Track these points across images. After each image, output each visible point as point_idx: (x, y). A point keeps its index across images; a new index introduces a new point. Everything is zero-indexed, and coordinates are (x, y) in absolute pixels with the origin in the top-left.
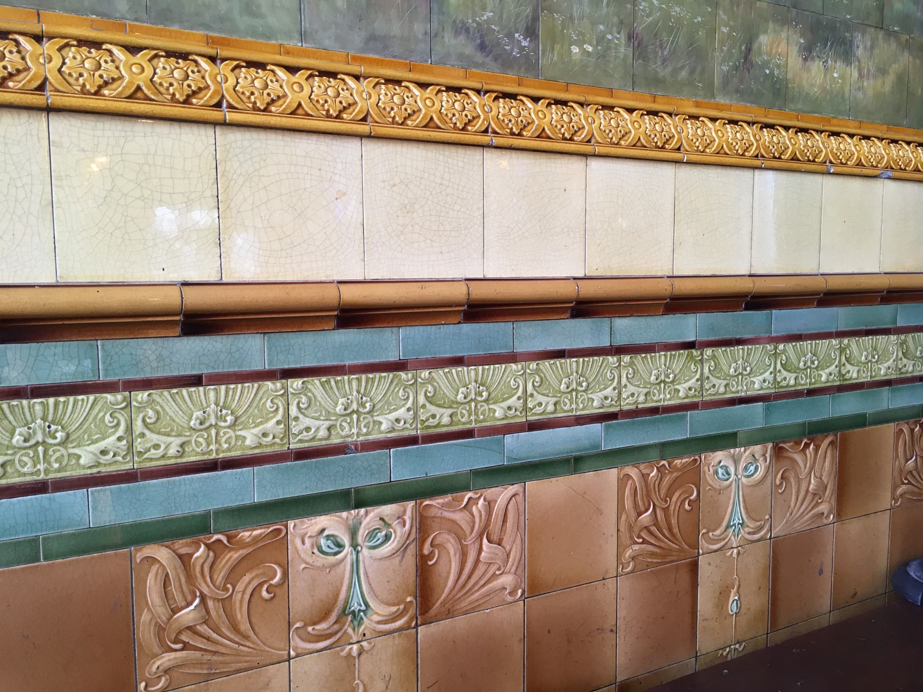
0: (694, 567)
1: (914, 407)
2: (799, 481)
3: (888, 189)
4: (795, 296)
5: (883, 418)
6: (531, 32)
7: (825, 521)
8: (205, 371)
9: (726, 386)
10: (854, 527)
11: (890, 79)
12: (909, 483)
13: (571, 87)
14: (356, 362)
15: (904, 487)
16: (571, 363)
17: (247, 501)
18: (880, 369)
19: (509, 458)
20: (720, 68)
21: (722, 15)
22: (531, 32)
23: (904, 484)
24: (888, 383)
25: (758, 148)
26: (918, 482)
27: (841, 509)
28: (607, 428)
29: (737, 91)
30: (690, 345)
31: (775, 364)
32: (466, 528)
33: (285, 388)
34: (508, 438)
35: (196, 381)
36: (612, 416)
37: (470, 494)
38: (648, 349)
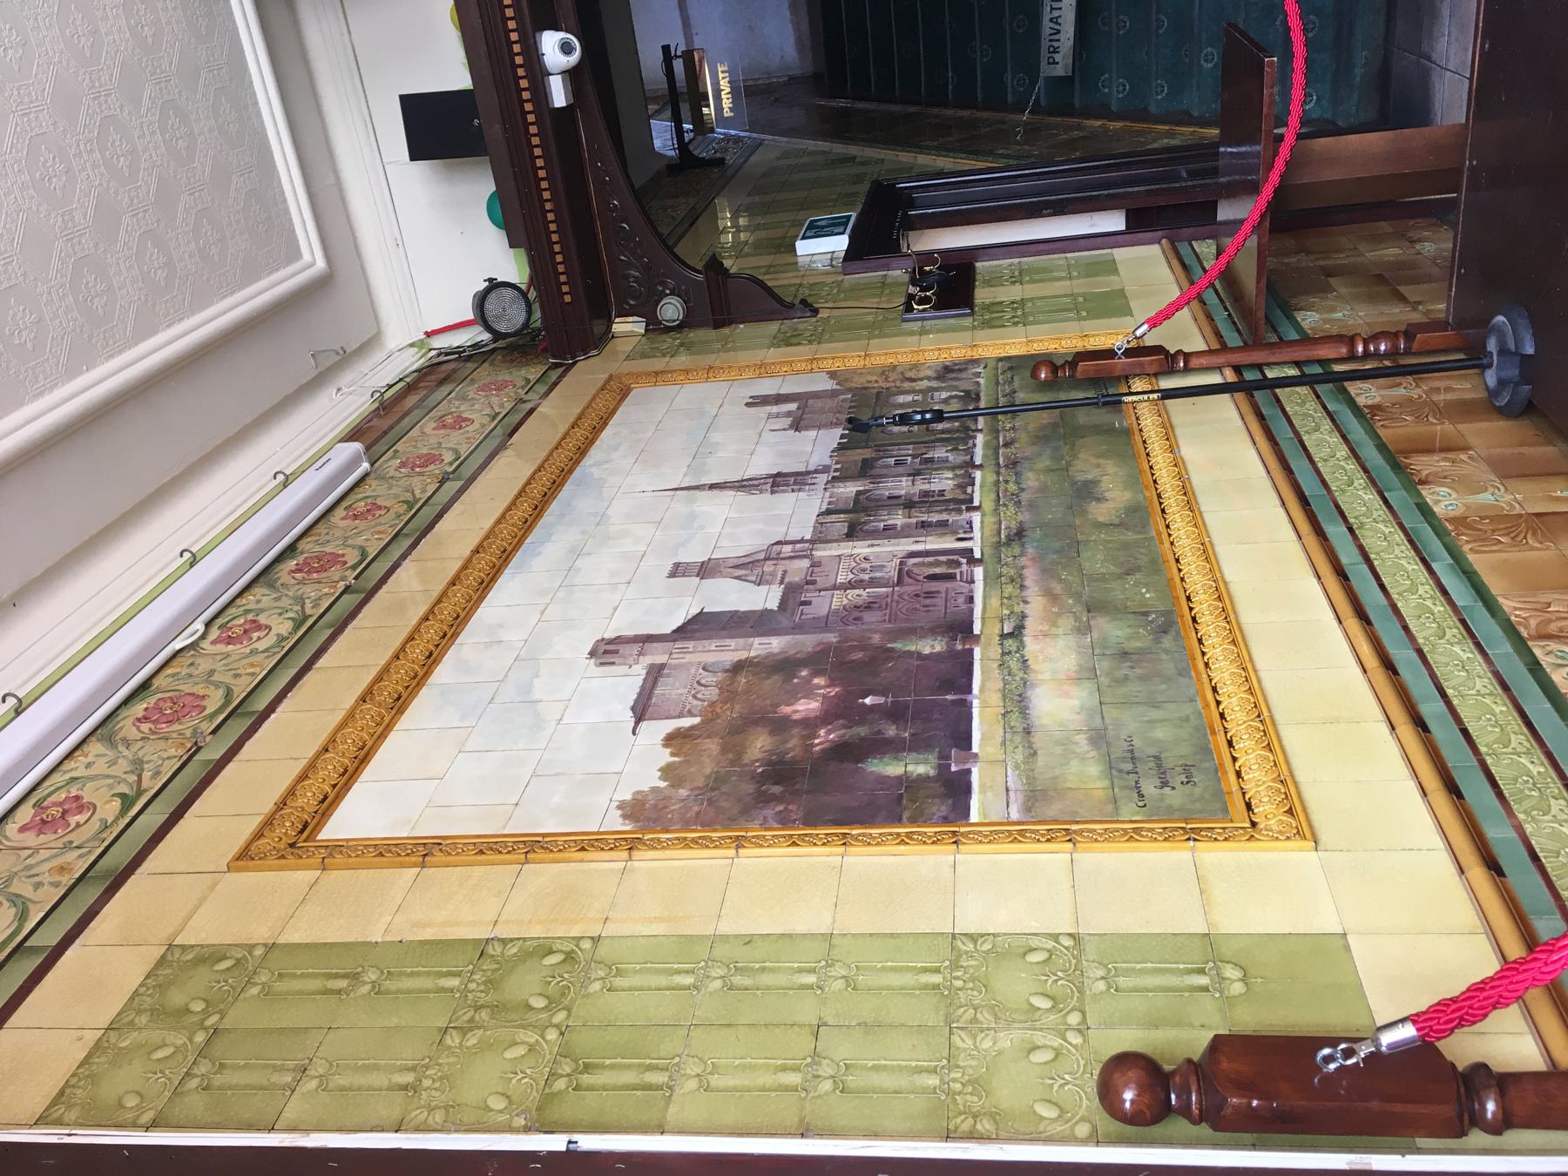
0: (1538, 515)
1: (1359, 422)
2: (1443, 471)
3: (1187, 451)
4: (1550, 991)
5: (1375, 436)
6: (1146, 614)
7: (1475, 455)
8: (1456, 728)
9: (1422, 584)
10: (1472, 441)
11: (1101, 461)
12: (1525, 538)
13: (1174, 594)
14: (1471, 753)
15: (1530, 542)
16: (1386, 581)
17: (1552, 710)
18: (1501, 712)
19: (1476, 601)
20: (1130, 536)
21: (1093, 538)
22: (1146, 614)
23: (1527, 543)
24: (1344, 437)
25: (1252, 720)
26: (1520, 532)
27: (1465, 448)
28: (1349, 433)
29: (1144, 527)
30: (1351, 529)
31: (1507, 754)
32: (1538, 620)
33: (1359, 528)
34: (1459, 603)
35: (1465, 732)
36: (1423, 560)
37: (1513, 618)
38: (1361, 549)
